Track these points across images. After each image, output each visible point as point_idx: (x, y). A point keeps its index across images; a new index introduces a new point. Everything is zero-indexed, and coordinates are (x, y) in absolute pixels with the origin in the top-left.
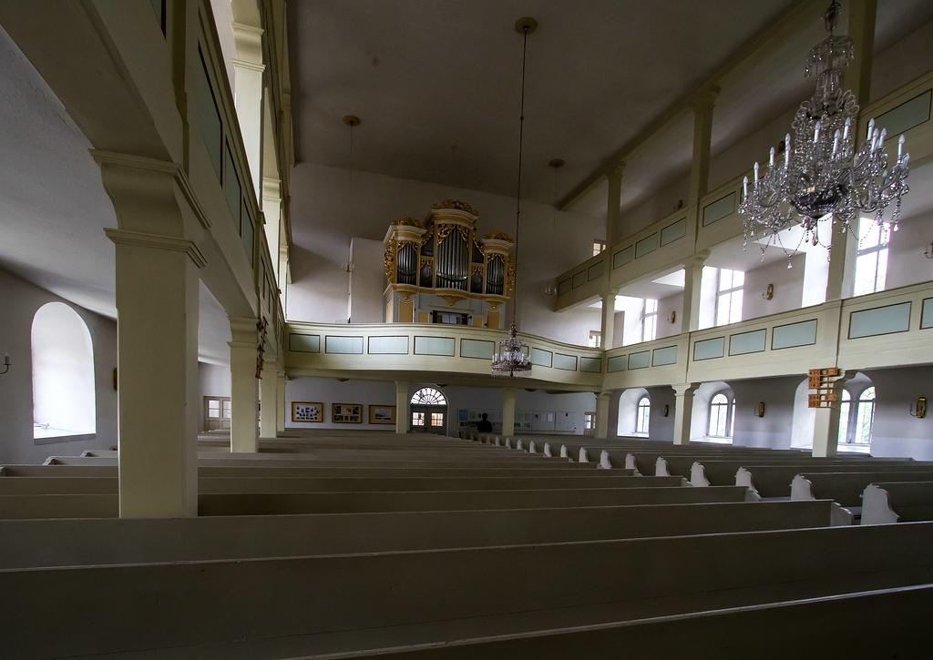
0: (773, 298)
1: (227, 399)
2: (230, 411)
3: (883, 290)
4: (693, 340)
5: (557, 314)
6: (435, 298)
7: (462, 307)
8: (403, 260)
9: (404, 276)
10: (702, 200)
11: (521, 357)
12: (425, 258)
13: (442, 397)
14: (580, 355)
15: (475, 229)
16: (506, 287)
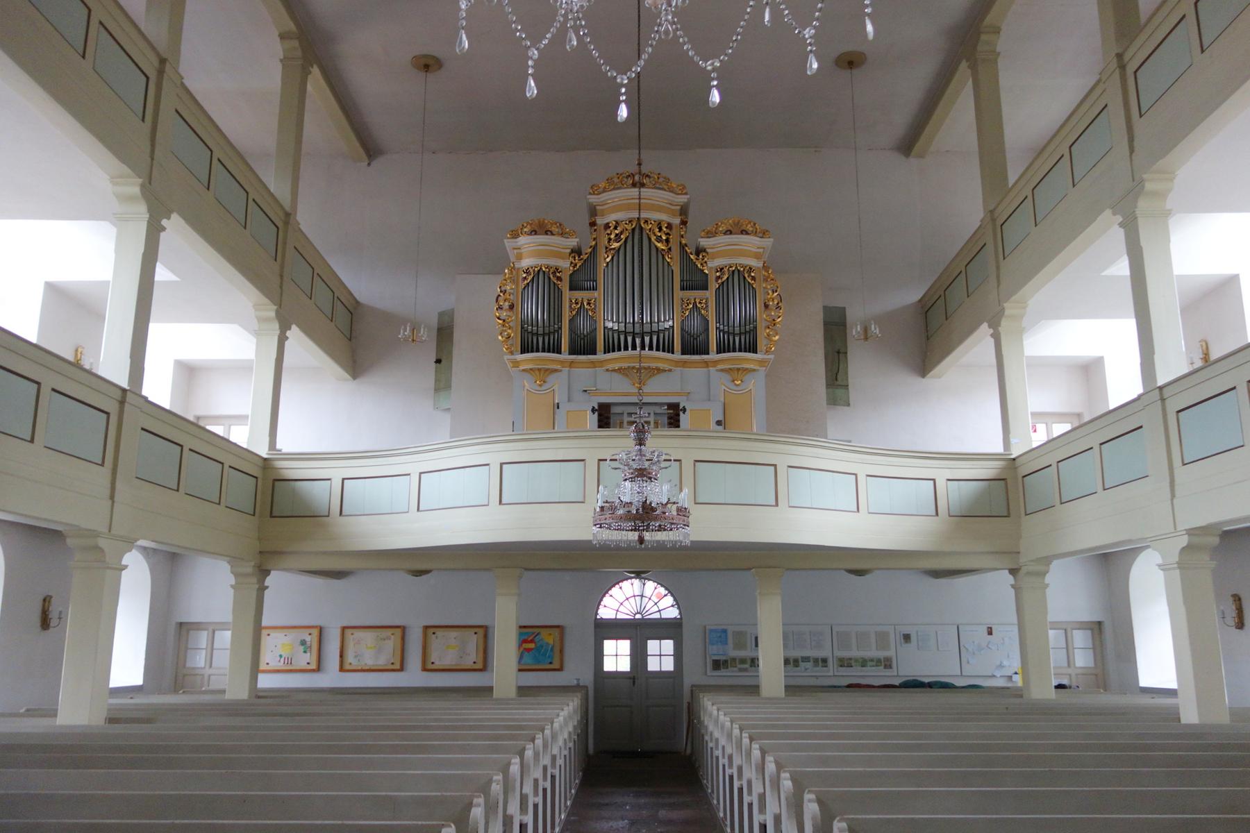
1: (223, 626)
2: (1052, 643)
4: (1173, 405)
5: (928, 381)
6: (605, 377)
7: (661, 389)
8: (533, 310)
9: (534, 340)
10: (1126, 57)
11: (658, 492)
12: (579, 295)
13: (669, 600)
14: (942, 472)
15: (684, 223)
16: (762, 334)
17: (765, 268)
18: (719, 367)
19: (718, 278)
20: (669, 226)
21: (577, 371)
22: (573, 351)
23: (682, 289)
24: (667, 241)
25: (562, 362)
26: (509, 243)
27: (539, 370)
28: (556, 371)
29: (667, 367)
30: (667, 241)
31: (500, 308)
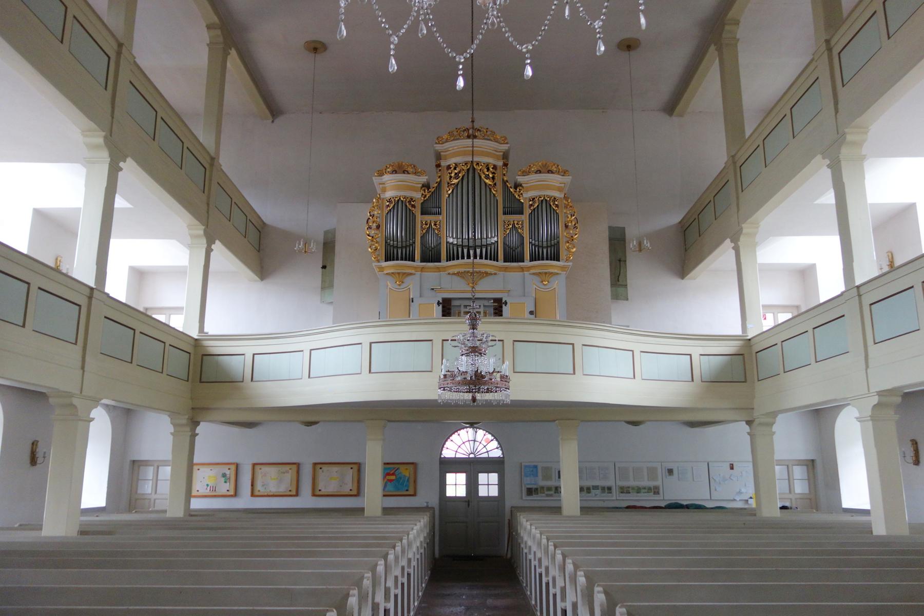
0: (31, 442)
1: (165, 463)
3: (876, 273)
4: (867, 299)
5: (686, 282)
6: (447, 279)
7: (488, 288)
8: (394, 229)
9: (395, 251)
10: (833, 42)
11: (486, 364)
12: (428, 218)
13: (495, 444)
14: (696, 349)
16: (563, 247)
17: (566, 198)
18: (532, 271)
19: (531, 205)
20: (495, 167)
21: (426, 274)
22: (423, 260)
23: (504, 213)
24: (493, 178)
25: (415, 268)
26: (376, 180)
27: (399, 273)
28: (411, 274)
29: (493, 271)
30: (493, 178)
31: (370, 228)
